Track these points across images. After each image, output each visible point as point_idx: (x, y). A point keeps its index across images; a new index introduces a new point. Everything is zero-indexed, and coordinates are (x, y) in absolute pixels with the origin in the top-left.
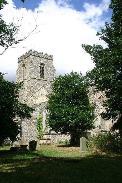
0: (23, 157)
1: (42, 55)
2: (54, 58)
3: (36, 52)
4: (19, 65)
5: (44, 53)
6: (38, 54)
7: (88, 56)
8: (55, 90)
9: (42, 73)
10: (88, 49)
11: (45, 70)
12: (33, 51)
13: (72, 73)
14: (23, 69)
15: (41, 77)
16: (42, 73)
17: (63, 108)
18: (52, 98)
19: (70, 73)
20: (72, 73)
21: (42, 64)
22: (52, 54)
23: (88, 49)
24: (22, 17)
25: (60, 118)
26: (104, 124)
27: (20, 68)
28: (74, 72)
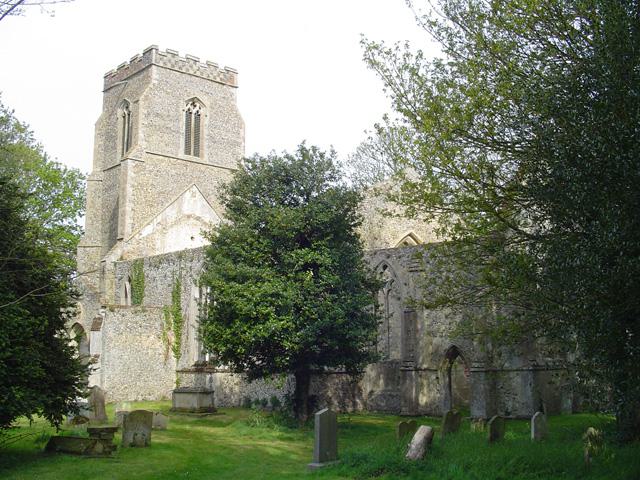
0: (267, 443)
1: (195, 68)
2: (240, 80)
3: (174, 55)
4: (105, 101)
5: (203, 61)
6: (181, 64)
7: (374, 80)
8: (236, 210)
9: (193, 140)
10: (373, 54)
11: (205, 122)
12: (162, 49)
13: (303, 150)
14: (121, 120)
15: (188, 152)
16: (193, 140)
17: (259, 279)
18: (222, 247)
19: (293, 151)
20: (303, 150)
21: (194, 102)
22: (231, 65)
23: (373, 54)
24: (192, 220)
25: (252, 320)
26: (412, 342)
27: (109, 111)
28: (308, 146)
